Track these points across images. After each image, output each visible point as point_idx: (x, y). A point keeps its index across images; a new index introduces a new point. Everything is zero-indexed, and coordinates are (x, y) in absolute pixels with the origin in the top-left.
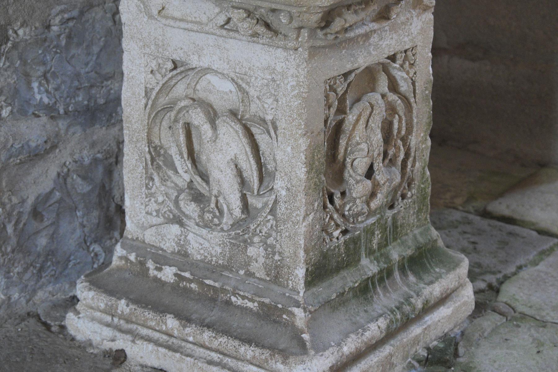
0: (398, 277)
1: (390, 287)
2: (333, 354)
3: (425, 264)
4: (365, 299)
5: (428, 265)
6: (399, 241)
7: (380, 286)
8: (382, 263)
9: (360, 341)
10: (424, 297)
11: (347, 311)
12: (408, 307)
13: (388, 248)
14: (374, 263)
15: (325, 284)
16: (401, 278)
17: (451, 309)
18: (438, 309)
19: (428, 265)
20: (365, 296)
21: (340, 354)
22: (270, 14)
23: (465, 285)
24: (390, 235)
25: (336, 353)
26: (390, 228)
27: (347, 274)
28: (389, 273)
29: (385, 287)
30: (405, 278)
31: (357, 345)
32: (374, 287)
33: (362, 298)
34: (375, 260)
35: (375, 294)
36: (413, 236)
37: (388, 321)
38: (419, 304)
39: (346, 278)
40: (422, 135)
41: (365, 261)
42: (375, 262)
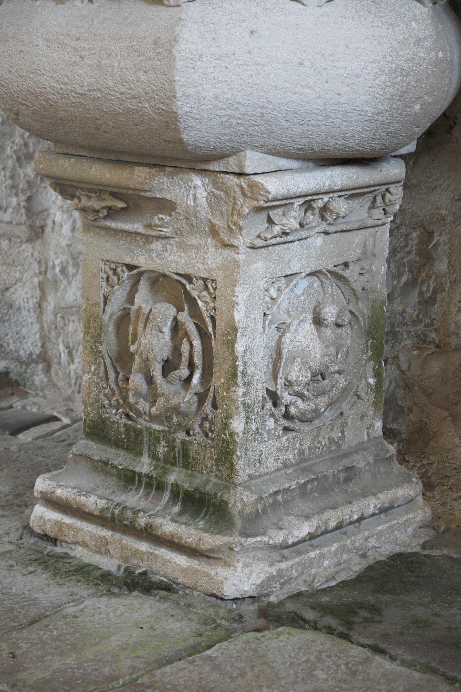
0: (167, 498)
1: (153, 497)
2: (49, 485)
3: (201, 512)
4: (125, 486)
5: (202, 515)
6: (190, 471)
7: (145, 489)
8: (156, 472)
9: (73, 496)
10: (151, 520)
11: (104, 480)
12: (131, 514)
13: (174, 468)
14: (151, 467)
15: (100, 446)
16: (168, 501)
17: (187, 564)
18: (181, 555)
19: (202, 515)
20: (127, 484)
21: (52, 490)
22: (335, 268)
23: (229, 566)
24: (179, 457)
25: (51, 487)
26: (179, 449)
27: (124, 455)
28: (160, 487)
29: (149, 494)
30: (171, 503)
31: (69, 497)
32: (140, 486)
33: (123, 484)
34: (154, 465)
35: (136, 491)
36: (206, 479)
37: (106, 506)
38: (142, 521)
39: (120, 456)
40: (223, 380)
41: (145, 459)
42: (153, 467)
